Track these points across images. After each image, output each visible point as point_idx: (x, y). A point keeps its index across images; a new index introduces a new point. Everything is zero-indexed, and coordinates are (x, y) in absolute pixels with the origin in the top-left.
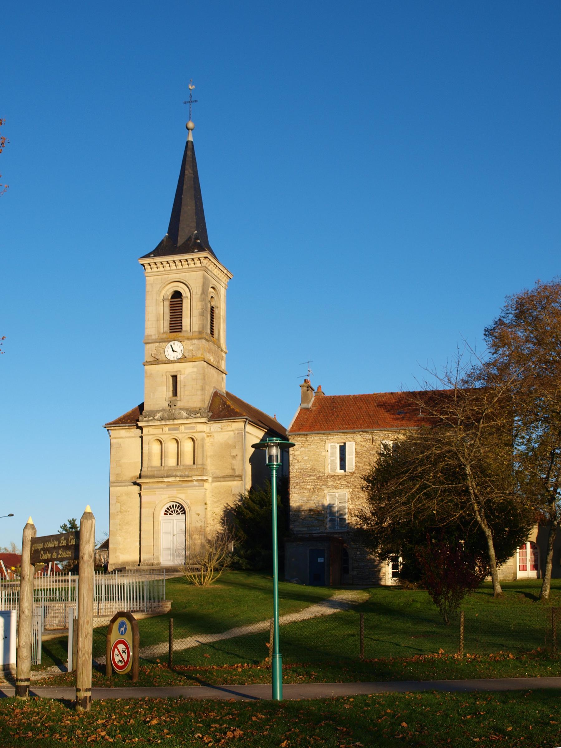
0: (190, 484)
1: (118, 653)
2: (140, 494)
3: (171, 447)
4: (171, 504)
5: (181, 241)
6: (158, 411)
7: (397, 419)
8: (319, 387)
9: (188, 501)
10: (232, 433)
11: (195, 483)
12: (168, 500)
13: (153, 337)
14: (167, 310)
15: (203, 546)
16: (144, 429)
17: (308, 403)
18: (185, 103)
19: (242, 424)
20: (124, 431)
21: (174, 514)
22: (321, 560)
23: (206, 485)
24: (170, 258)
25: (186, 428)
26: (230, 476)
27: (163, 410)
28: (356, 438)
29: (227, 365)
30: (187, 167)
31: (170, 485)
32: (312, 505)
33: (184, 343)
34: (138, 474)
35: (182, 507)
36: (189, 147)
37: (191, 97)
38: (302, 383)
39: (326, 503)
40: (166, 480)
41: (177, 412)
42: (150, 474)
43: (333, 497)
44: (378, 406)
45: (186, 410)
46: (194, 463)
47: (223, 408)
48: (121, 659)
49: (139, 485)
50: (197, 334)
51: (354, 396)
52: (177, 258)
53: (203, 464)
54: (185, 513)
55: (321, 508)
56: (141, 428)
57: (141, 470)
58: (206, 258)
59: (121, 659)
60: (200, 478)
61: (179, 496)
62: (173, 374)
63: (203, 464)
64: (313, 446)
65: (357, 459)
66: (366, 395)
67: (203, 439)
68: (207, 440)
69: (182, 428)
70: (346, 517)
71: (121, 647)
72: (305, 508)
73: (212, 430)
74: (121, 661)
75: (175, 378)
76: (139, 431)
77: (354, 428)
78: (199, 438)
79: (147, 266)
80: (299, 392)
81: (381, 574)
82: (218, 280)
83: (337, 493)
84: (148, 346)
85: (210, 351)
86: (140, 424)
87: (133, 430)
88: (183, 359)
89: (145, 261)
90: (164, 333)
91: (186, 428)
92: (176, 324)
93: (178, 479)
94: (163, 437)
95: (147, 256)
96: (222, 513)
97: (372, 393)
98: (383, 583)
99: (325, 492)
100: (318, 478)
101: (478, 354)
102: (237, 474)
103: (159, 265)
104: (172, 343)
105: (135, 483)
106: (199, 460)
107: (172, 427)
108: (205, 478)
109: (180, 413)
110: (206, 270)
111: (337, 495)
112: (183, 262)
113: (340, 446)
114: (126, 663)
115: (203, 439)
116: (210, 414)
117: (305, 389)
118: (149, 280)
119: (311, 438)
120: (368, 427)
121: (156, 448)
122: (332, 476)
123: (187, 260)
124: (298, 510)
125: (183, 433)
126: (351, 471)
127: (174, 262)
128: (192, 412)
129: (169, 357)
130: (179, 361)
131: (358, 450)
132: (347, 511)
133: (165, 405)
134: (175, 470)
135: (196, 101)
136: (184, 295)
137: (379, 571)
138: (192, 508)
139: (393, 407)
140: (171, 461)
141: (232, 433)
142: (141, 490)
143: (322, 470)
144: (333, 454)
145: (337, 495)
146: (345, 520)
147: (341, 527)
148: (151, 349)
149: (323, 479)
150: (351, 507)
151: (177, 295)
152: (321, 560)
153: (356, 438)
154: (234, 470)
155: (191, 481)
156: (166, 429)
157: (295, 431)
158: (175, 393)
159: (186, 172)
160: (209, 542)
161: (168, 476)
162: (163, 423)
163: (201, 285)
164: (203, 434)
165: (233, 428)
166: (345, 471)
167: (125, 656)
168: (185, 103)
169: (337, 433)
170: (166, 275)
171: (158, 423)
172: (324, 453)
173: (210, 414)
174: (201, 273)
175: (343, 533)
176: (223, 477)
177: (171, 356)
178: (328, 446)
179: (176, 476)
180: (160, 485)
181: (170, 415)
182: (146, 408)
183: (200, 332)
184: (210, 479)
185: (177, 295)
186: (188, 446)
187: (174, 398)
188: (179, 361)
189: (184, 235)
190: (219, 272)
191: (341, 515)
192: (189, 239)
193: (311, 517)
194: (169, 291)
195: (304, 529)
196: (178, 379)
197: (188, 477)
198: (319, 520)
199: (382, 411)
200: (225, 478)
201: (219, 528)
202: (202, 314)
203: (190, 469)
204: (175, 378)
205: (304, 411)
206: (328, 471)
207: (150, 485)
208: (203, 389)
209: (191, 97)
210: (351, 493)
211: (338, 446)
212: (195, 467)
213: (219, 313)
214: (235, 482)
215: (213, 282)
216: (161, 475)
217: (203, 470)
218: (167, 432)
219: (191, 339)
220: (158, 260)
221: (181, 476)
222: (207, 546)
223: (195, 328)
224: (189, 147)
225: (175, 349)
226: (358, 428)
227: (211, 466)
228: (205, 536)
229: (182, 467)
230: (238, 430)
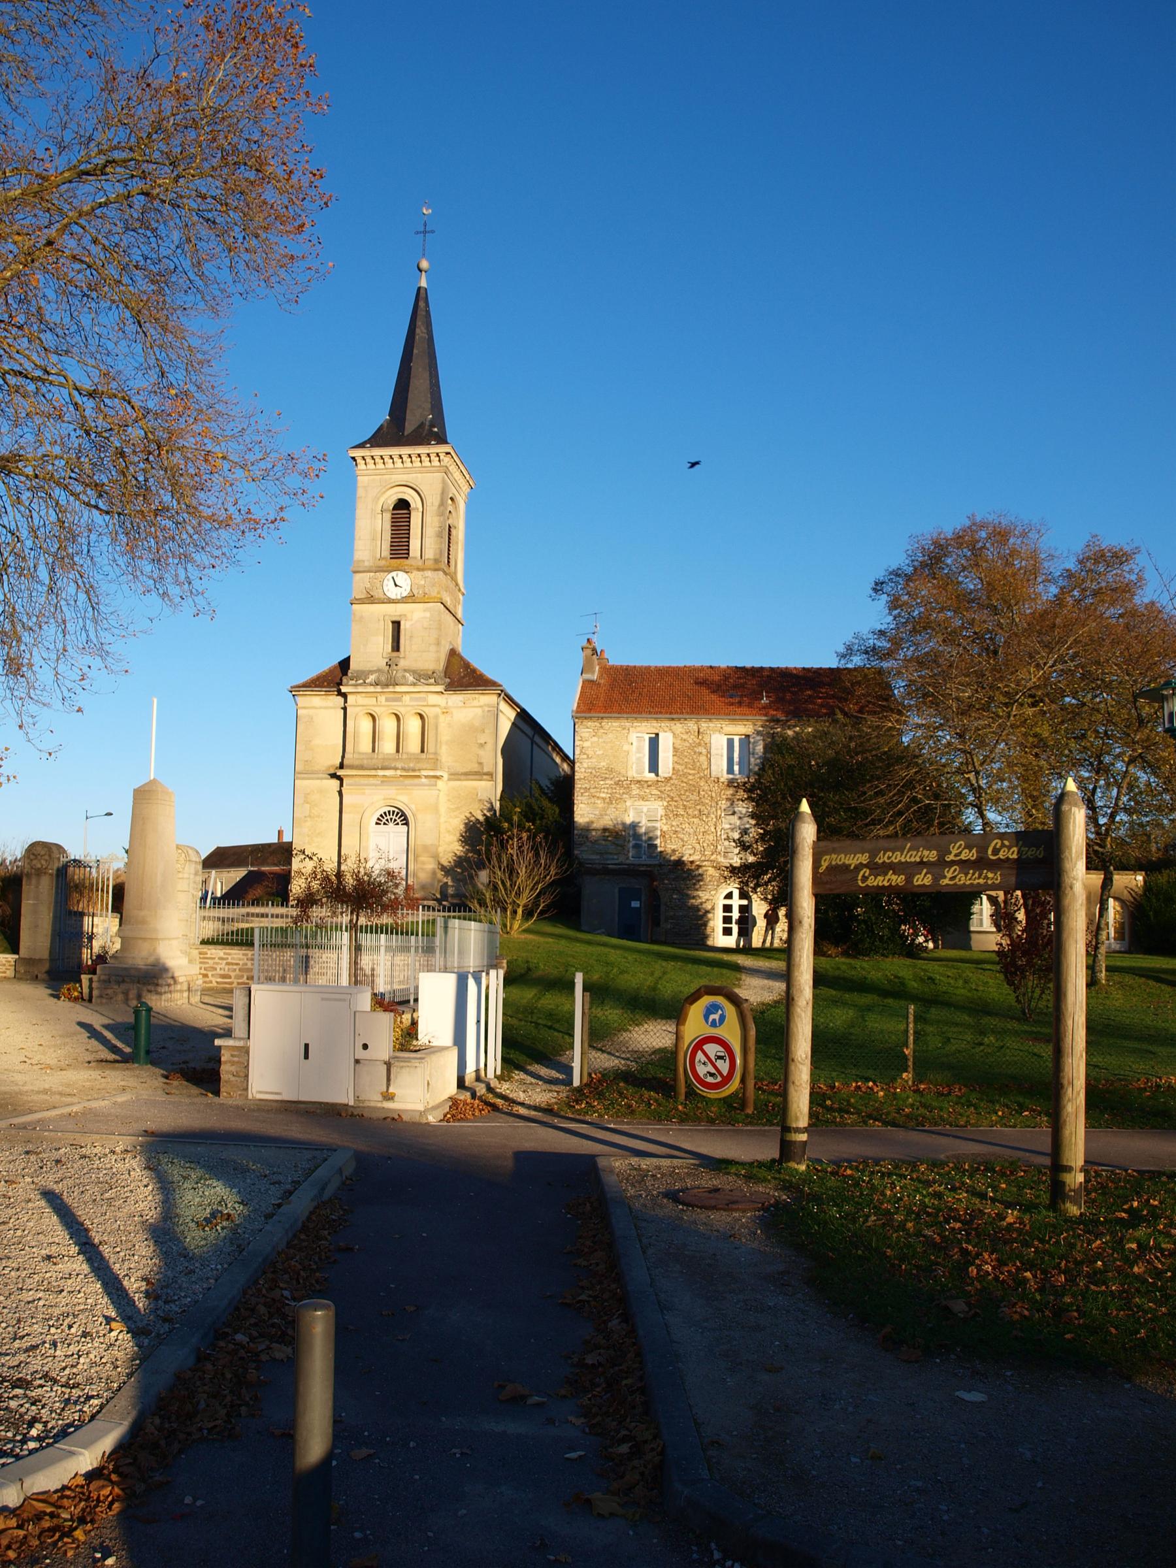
0: (416, 781)
1: (703, 1059)
2: (340, 793)
3: (388, 726)
4: (386, 809)
5: (409, 428)
6: (371, 672)
7: (732, 704)
8: (602, 651)
9: (413, 807)
10: (479, 711)
11: (424, 780)
12: (382, 803)
13: (367, 564)
14: (388, 526)
15: (434, 873)
16: (349, 698)
17: (593, 673)
18: (417, 233)
19: (495, 698)
20: (318, 698)
21: (391, 824)
22: (635, 904)
23: (440, 783)
24: (395, 451)
25: (411, 699)
26: (476, 773)
27: (379, 671)
28: (674, 728)
29: (464, 611)
30: (419, 323)
31: (386, 780)
32: (607, 821)
33: (412, 576)
34: (338, 761)
35: (403, 814)
36: (421, 296)
37: (425, 225)
38: (585, 643)
39: (628, 820)
40: (381, 773)
41: (400, 674)
42: (357, 763)
43: (639, 812)
44: (696, 683)
45: (414, 672)
46: (422, 751)
47: (462, 676)
48: (713, 1071)
49: (340, 778)
50: (431, 562)
51: (804, 669)
52: (405, 451)
53: (435, 753)
54: (407, 824)
55: (620, 827)
56: (344, 696)
57: (343, 757)
58: (448, 453)
59: (713, 1071)
60: (432, 773)
61: (399, 798)
62: (394, 619)
63: (435, 753)
64: (610, 735)
65: (676, 759)
66: (641, 667)
67: (437, 717)
68: (442, 718)
69: (406, 698)
70: (658, 842)
71: (712, 1049)
72: (594, 825)
73: (450, 704)
74: (712, 1075)
75: (397, 625)
76: (341, 699)
77: (671, 713)
78: (431, 715)
79: (359, 461)
80: (579, 659)
81: (709, 930)
82: (458, 488)
83: (645, 806)
84: (358, 576)
85: (447, 589)
86: (344, 689)
87: (331, 697)
88: (410, 598)
89: (357, 453)
90: (381, 558)
91: (411, 699)
92: (400, 547)
93: (399, 773)
94: (377, 711)
95: (361, 446)
96: (462, 827)
97: (681, 665)
98: (710, 943)
99: (628, 804)
100: (617, 784)
101: (872, 617)
102: (485, 770)
103: (378, 460)
104: (394, 574)
105: (334, 776)
106: (430, 746)
107: (392, 696)
108: (438, 773)
109: (404, 677)
110: (447, 472)
111: (645, 810)
112: (423, 458)
113: (650, 739)
114: (727, 1079)
115: (437, 717)
116: (448, 680)
117: (589, 652)
118: (362, 480)
119: (609, 724)
120: (692, 713)
121: (366, 725)
122: (639, 782)
123: (419, 455)
124: (587, 829)
125: (408, 705)
126: (666, 775)
127: (401, 457)
128: (422, 677)
129: (389, 594)
130: (404, 600)
131: (677, 746)
132: (659, 833)
133: (382, 663)
134: (395, 760)
135: (433, 232)
136: (413, 505)
137: (705, 925)
138: (419, 816)
139: (719, 686)
140: (388, 746)
141: (479, 711)
142: (341, 785)
143: (623, 772)
144: (639, 750)
145: (645, 810)
146: (656, 846)
147: (650, 857)
148: (361, 582)
149: (624, 785)
150: (665, 828)
151: (402, 505)
152: (635, 904)
153: (674, 728)
154: (480, 764)
155: (419, 777)
156: (382, 698)
157: (583, 712)
158: (396, 647)
159: (418, 331)
160: (443, 868)
161: (383, 769)
162: (379, 689)
163: (439, 492)
164: (438, 710)
165: (482, 703)
166: (657, 775)
167: (724, 1067)
168: (417, 233)
169: (647, 719)
170: (384, 476)
171: (371, 689)
172: (626, 747)
173: (448, 680)
174: (439, 476)
175: (655, 865)
176: (466, 774)
177: (392, 592)
178: (633, 737)
179: (396, 769)
180: (372, 781)
181: (388, 680)
182: (353, 665)
183: (436, 561)
184: (446, 776)
185: (402, 505)
186: (413, 726)
187: (395, 654)
188: (404, 600)
189: (410, 420)
190: (461, 477)
191: (650, 839)
192: (422, 425)
193: (605, 839)
194: (391, 497)
195: (594, 857)
196: (402, 627)
197: (414, 770)
198: (617, 845)
199: (705, 691)
200: (468, 775)
201: (458, 848)
202: (439, 535)
203: (412, 758)
204: (397, 625)
205: (587, 684)
206: (632, 773)
207: (357, 779)
208: (438, 644)
209: (425, 225)
210: (666, 808)
211: (647, 737)
212: (424, 756)
213: (457, 536)
214: (483, 783)
215: (452, 491)
216: (373, 766)
217: (436, 763)
218: (384, 702)
219: (423, 570)
220: (377, 452)
221: (403, 769)
222: (440, 874)
223: (429, 554)
224: (421, 296)
225: (399, 583)
226: (677, 713)
227: (447, 757)
228: (436, 856)
229: (405, 756)
230: (489, 706)
